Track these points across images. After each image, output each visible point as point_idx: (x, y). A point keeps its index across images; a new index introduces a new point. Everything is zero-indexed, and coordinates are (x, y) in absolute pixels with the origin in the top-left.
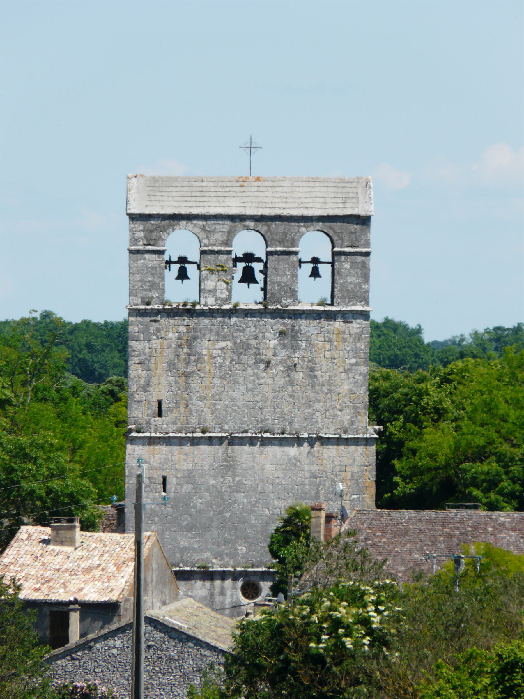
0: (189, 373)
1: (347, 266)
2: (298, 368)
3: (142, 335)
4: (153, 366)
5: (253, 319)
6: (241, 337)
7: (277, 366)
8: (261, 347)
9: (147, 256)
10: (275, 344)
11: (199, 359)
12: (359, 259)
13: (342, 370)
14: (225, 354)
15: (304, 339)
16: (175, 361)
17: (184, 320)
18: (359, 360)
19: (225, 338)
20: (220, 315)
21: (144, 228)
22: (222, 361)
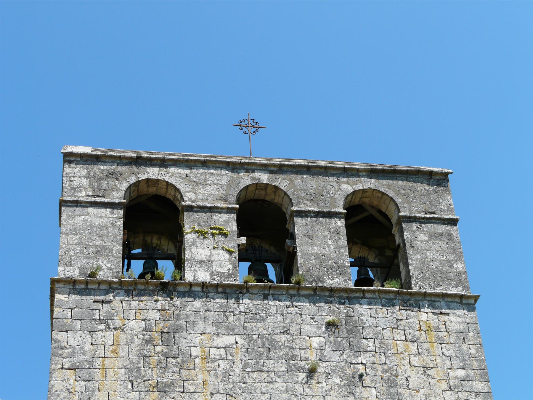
0: (166, 385)
1: (423, 237)
2: (367, 380)
3: (79, 323)
4: (97, 374)
5: (277, 302)
6: (258, 329)
7: (328, 376)
8: (297, 344)
9: (91, 210)
10: (321, 342)
11: (185, 362)
12: (442, 228)
13: (445, 386)
14: (232, 355)
15: (371, 335)
16: (141, 365)
17: (157, 301)
18: (472, 373)
19: (230, 331)
20: (220, 295)
21: (89, 173)
22: (228, 366)
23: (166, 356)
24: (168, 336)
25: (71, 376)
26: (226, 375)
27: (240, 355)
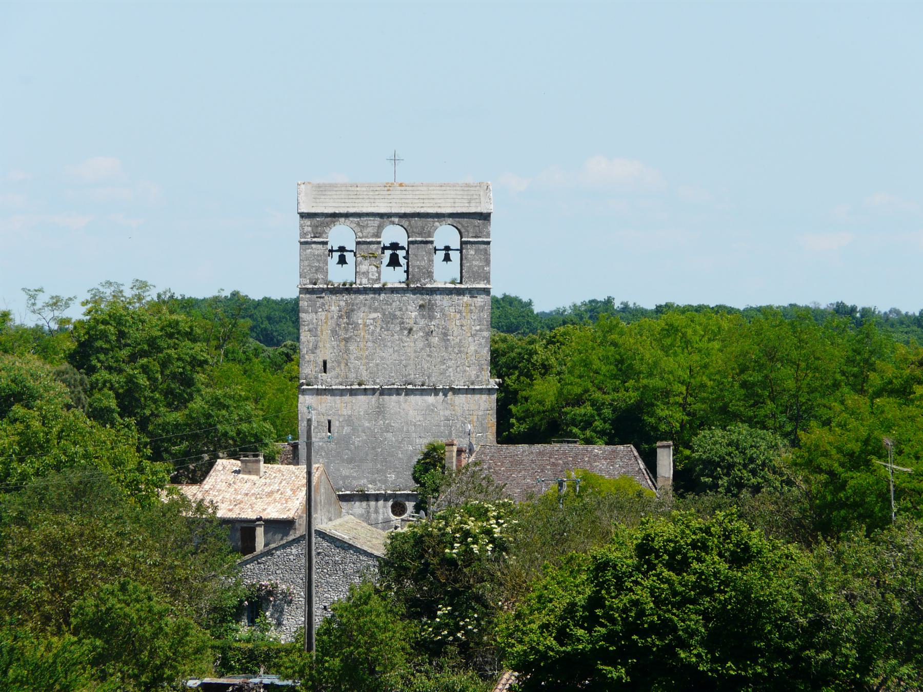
1: (472, 252)
6: (389, 309)
9: (314, 246)
11: (356, 326)
18: (483, 327)
19: (376, 310)
23: (348, 324)
24: (349, 314)
25: (308, 334)
26: (373, 333)
27: (379, 322)
